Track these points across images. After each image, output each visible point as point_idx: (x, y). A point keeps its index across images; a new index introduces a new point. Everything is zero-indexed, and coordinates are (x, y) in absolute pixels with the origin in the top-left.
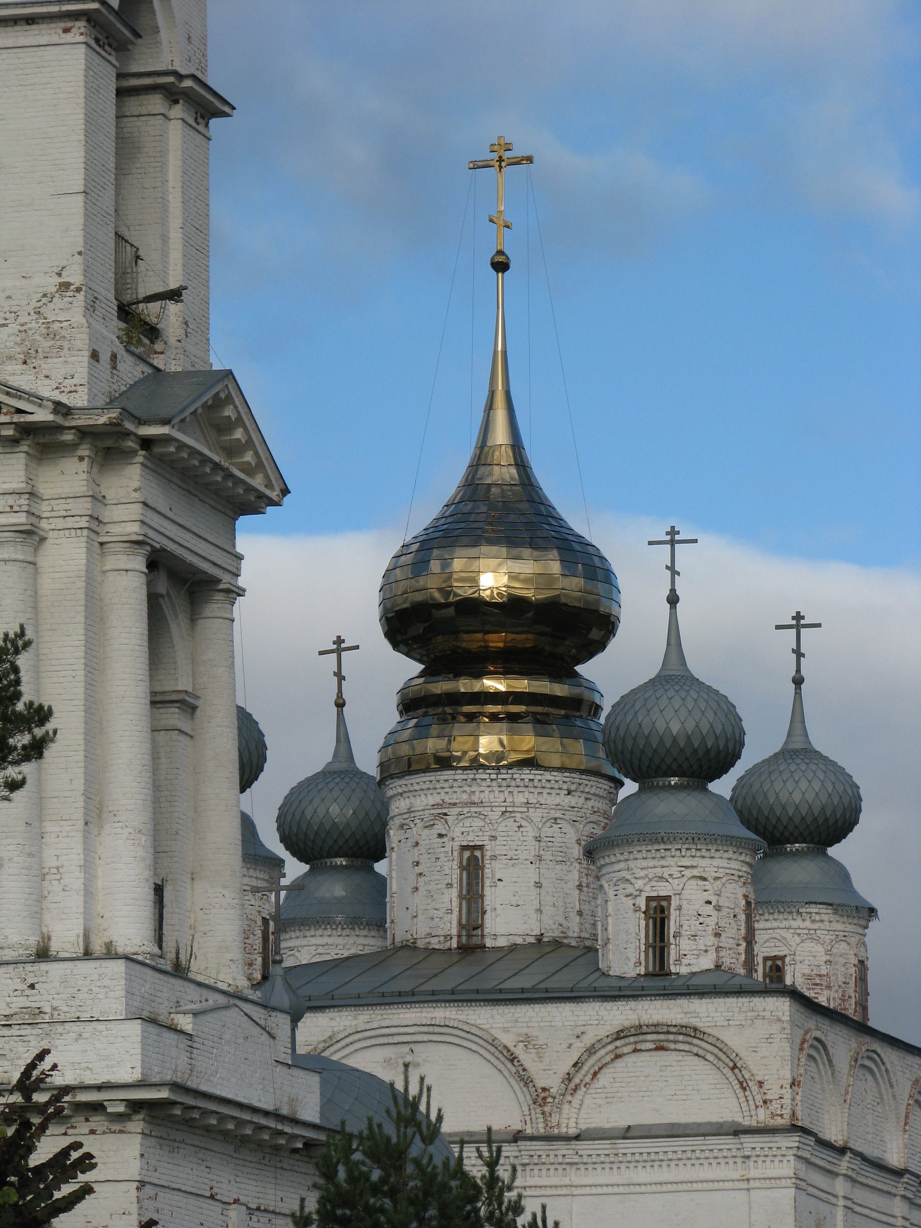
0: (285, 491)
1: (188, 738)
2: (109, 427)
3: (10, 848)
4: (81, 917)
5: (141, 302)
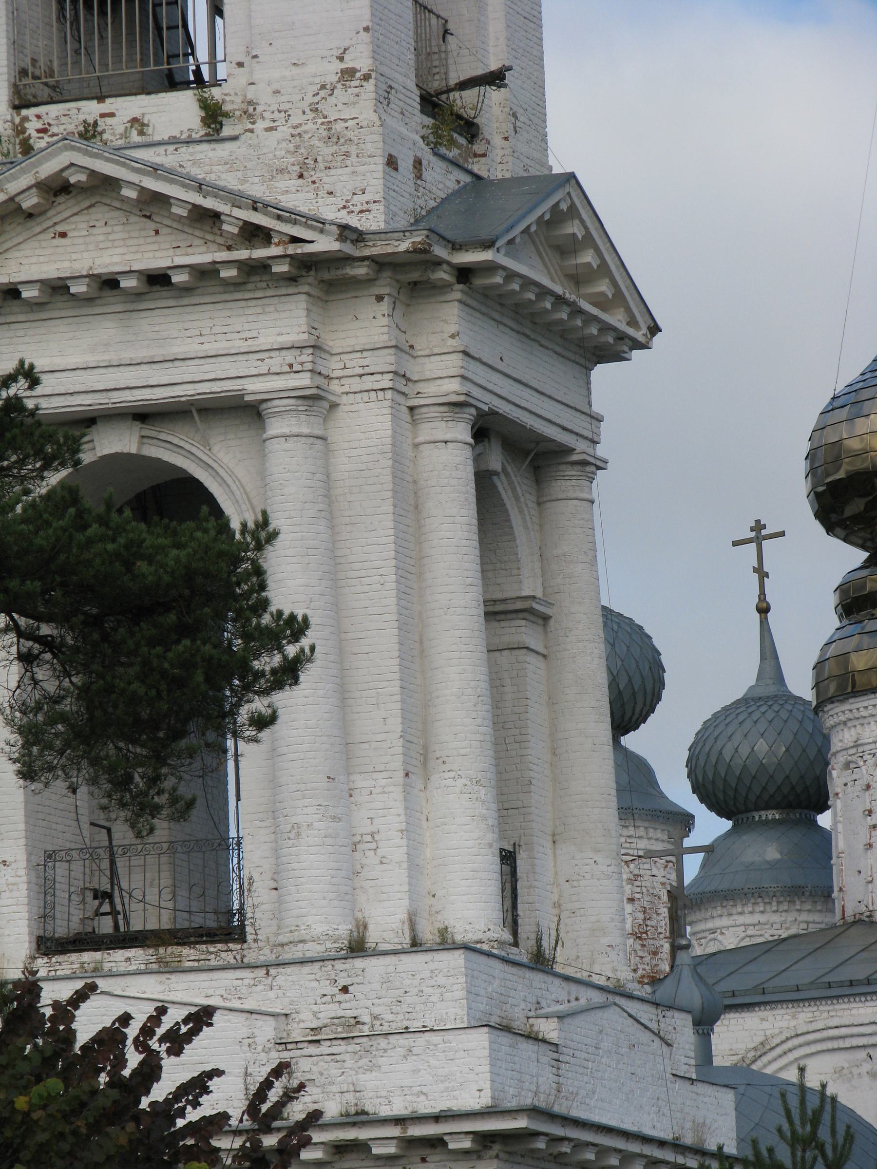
0: (655, 329)
1: (541, 658)
2: (414, 255)
3: (310, 810)
4: (406, 896)
5: (452, 90)
